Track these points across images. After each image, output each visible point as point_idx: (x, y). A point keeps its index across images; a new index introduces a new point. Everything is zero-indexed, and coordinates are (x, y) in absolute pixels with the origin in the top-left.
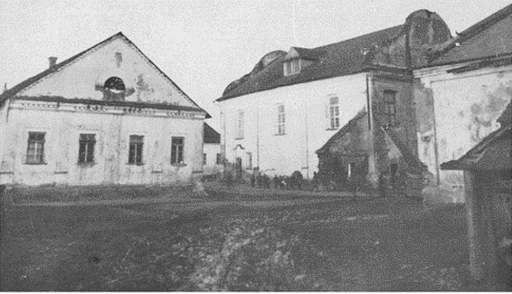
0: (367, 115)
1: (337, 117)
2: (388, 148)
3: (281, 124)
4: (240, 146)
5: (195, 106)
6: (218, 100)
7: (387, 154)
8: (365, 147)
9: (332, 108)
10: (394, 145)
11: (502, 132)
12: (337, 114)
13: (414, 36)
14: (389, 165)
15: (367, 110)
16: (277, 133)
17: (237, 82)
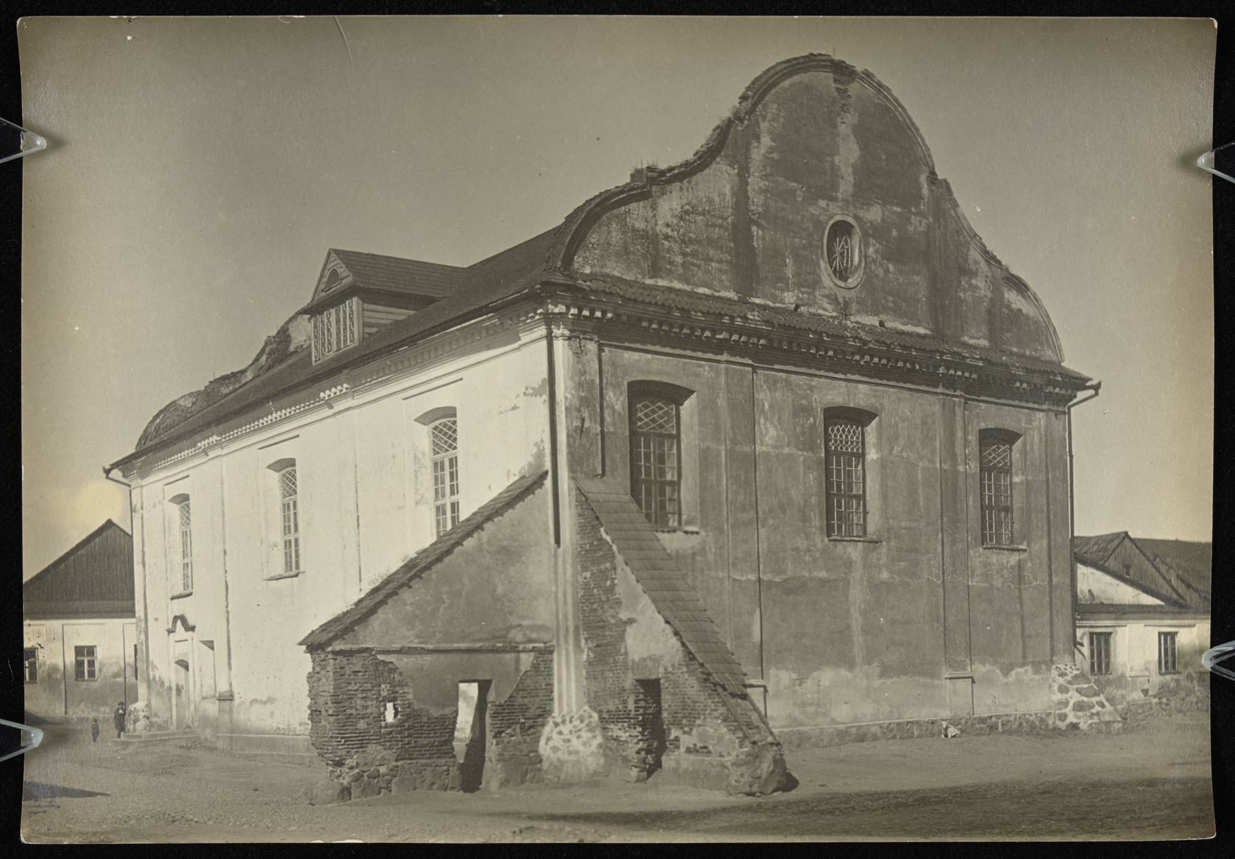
0: (548, 483)
1: (454, 498)
2: (624, 616)
3: (292, 537)
4: (183, 619)
5: (338, 646)
6: (125, 464)
7: (622, 638)
8: (543, 613)
9: (438, 466)
10: (645, 600)
11: (766, 141)
12: (454, 490)
13: (773, 166)
14: (629, 682)
15: (548, 465)
16: (280, 569)
17: (188, 403)
